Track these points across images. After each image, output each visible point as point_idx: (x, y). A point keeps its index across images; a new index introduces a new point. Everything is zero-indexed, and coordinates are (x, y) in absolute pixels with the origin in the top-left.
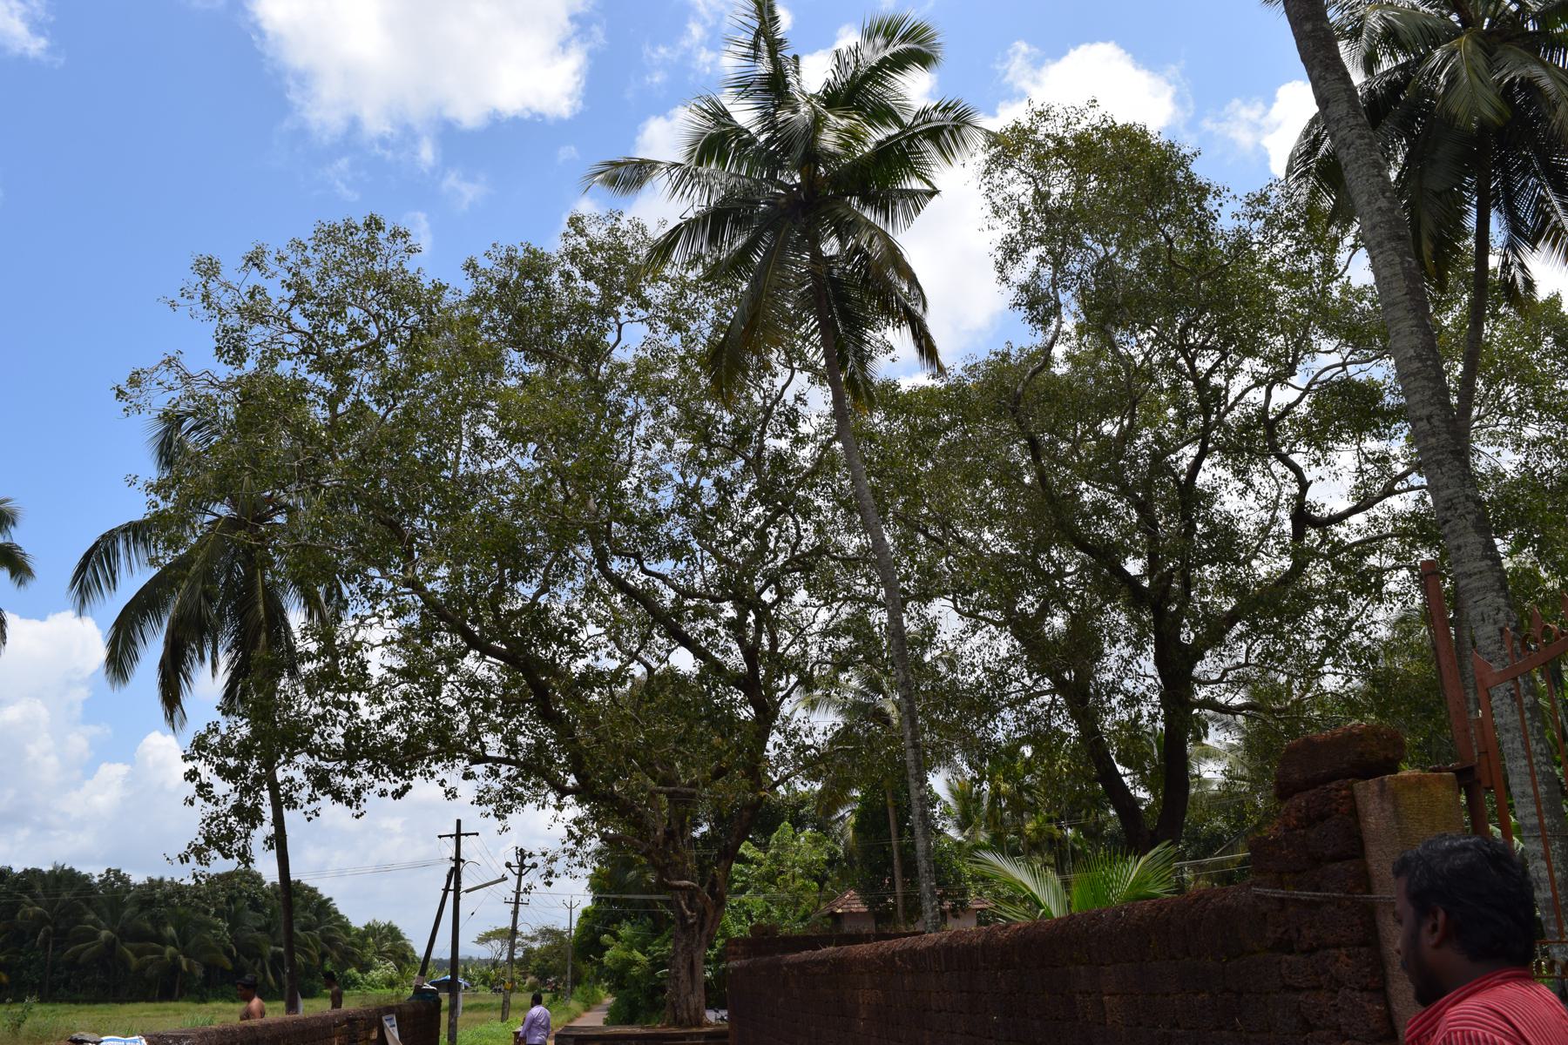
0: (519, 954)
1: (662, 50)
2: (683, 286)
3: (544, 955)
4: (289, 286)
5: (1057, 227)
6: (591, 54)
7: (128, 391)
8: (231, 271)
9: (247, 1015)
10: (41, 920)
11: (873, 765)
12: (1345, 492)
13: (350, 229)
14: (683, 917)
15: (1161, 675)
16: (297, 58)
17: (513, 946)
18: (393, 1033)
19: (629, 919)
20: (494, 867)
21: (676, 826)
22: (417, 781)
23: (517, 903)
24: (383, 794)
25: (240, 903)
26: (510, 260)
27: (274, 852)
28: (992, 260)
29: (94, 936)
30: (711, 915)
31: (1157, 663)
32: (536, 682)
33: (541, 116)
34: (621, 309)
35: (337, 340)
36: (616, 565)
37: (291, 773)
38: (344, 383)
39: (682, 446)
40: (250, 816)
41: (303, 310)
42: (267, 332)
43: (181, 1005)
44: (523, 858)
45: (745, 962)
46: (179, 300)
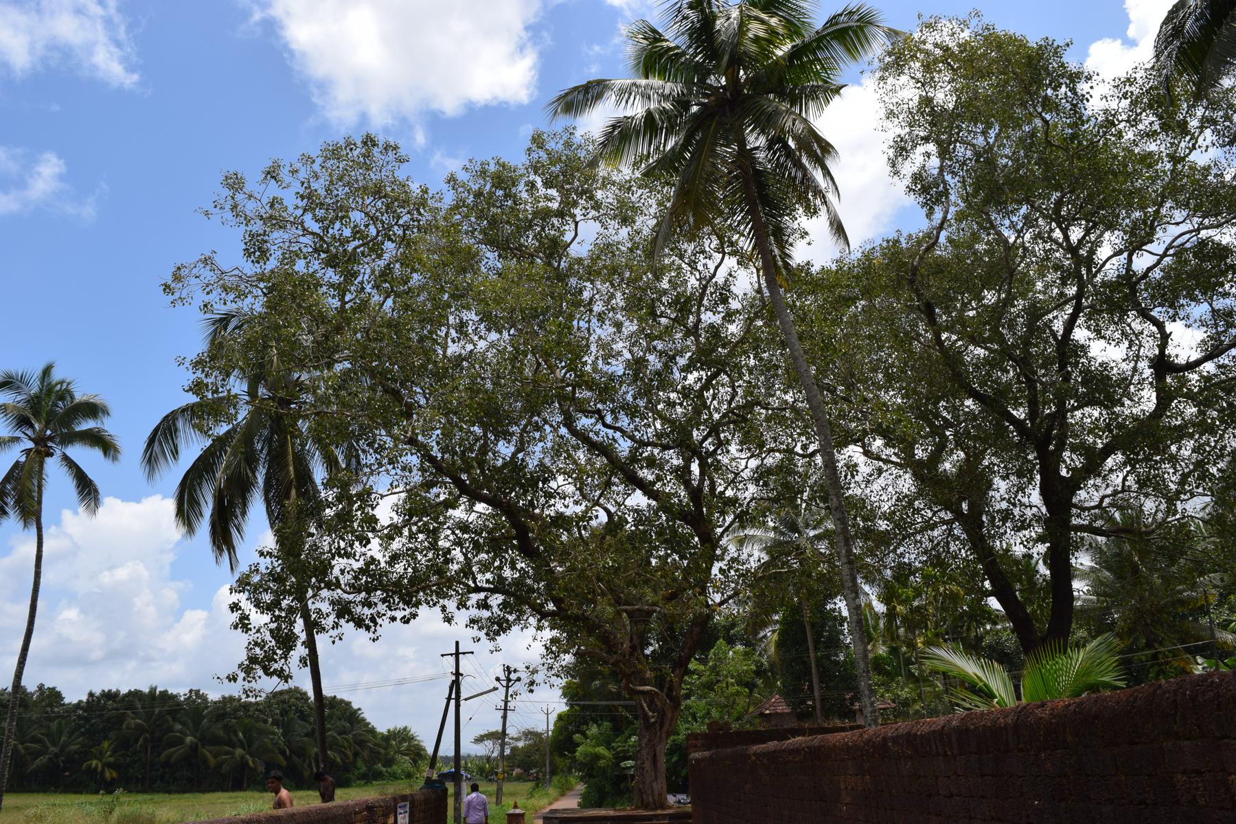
0: (507, 752)
1: (597, 48)
2: (626, 187)
3: (527, 752)
4: (302, 197)
5: (938, 125)
6: (541, 54)
7: (173, 285)
8: (253, 183)
9: (280, 804)
10: (140, 729)
11: (791, 589)
12: (1194, 345)
13: (350, 145)
14: (646, 718)
15: (1046, 504)
16: (319, 69)
17: (503, 745)
18: (403, 820)
19: (596, 722)
20: (488, 681)
21: (636, 641)
22: (423, 610)
23: (505, 709)
24: (393, 619)
25: (291, 715)
26: (483, 173)
27: (308, 669)
28: (886, 157)
29: (181, 742)
30: (669, 715)
31: (1042, 493)
32: (519, 530)
33: (506, 103)
34: (577, 212)
35: (344, 242)
36: (584, 422)
37: (318, 605)
38: (350, 275)
39: (630, 327)
40: (286, 641)
41: (314, 215)
42: (286, 236)
43: (248, 794)
44: (510, 673)
45: (707, 754)
46: (212, 210)
